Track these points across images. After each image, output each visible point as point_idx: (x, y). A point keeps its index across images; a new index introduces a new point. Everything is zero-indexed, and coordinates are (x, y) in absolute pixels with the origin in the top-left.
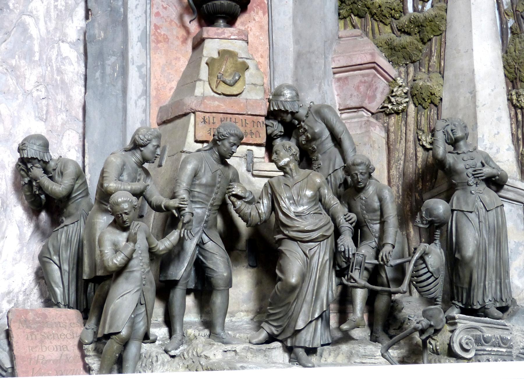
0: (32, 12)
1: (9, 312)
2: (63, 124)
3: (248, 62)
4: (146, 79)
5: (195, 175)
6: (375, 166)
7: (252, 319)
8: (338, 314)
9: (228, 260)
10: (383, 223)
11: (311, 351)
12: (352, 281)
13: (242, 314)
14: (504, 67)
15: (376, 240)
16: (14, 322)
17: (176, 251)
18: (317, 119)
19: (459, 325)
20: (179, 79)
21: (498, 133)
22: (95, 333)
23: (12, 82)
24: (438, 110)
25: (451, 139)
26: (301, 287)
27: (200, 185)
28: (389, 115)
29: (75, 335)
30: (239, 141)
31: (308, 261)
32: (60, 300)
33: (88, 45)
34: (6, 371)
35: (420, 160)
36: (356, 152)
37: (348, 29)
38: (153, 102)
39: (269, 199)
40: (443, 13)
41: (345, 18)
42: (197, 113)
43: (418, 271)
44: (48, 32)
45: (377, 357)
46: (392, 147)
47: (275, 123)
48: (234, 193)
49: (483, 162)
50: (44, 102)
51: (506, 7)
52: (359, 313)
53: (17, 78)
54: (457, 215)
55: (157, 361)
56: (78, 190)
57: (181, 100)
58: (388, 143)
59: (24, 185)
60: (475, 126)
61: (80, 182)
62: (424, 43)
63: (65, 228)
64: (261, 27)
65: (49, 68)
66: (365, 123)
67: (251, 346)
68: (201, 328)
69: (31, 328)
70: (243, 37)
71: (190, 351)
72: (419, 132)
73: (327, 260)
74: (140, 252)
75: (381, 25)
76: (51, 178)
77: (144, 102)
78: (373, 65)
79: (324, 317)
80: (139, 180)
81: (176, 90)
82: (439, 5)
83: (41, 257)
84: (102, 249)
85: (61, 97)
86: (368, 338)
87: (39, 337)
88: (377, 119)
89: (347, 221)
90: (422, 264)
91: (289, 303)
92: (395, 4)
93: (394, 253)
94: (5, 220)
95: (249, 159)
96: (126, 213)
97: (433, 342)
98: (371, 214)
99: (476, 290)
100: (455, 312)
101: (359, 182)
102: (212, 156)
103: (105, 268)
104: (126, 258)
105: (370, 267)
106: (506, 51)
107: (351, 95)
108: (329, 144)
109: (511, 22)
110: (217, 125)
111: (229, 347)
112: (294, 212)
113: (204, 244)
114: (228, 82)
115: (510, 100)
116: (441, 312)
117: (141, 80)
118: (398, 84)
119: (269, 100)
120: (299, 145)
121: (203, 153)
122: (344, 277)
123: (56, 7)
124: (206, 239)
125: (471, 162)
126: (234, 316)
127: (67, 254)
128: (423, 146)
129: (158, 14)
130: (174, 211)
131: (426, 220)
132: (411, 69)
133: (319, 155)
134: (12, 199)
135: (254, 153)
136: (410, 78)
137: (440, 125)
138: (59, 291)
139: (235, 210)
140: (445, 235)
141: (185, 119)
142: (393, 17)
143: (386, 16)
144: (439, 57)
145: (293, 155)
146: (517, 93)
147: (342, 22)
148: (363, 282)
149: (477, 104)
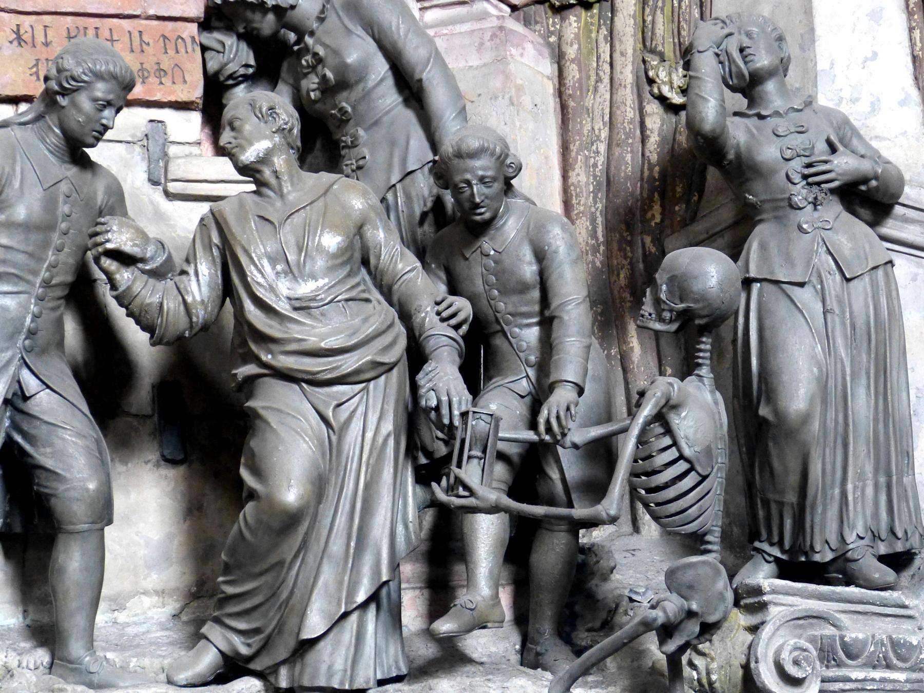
8: (426, 592)
9: (97, 442)
10: (547, 322)
12: (461, 491)
13: (147, 601)
15: (531, 373)
19: (773, 610)
25: (741, 75)
31: (334, 438)
35: (654, 139)
46: (572, 104)
47: (230, 41)
48: (109, 246)
49: (833, 138)
58: (560, 93)
72: (649, 57)
73: (388, 435)
86: (515, 658)
91: (281, 563)
97: (699, 662)
98: (515, 298)
100: (761, 575)
101: (478, 206)
102: (43, 140)
105: (513, 450)
110: (59, 46)
112: (289, 299)
113: (26, 398)
116: (718, 573)
120: (300, 104)
124: (31, 383)
125: (797, 141)
126: (121, 608)
131: (671, 311)
133: (361, 132)
139: (117, 298)
145: (280, 130)
148: (493, 495)
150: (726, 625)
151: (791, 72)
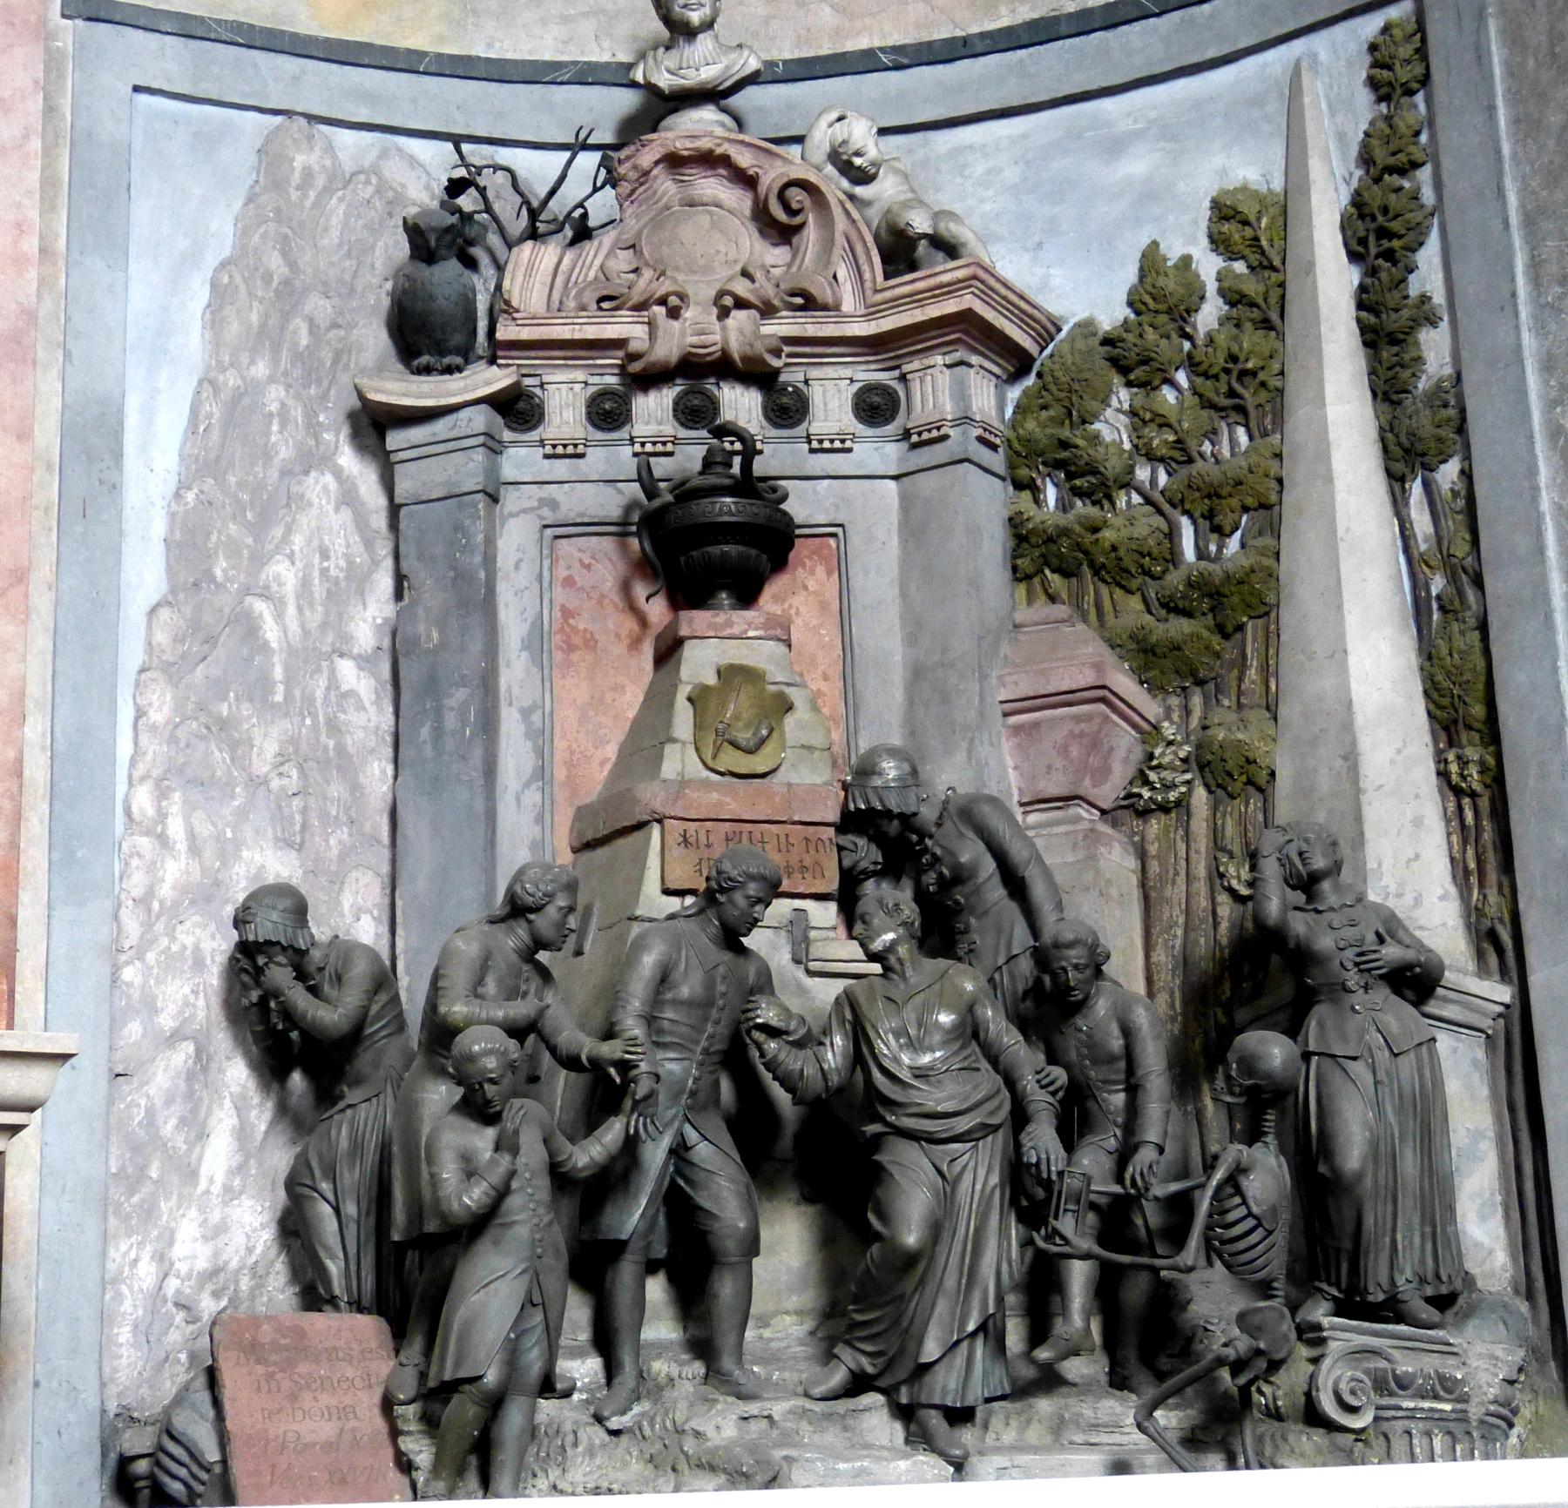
0: (267, 587)
1: (214, 1323)
2: (343, 855)
3: (792, 693)
4: (542, 739)
5: (664, 978)
6: (1110, 946)
7: (812, 1333)
8: (1027, 1320)
9: (747, 1186)
10: (1133, 1089)
11: (960, 1416)
12: (1058, 1241)
13: (788, 1319)
14: (1426, 693)
15: (1119, 1132)
16: (226, 1349)
17: (619, 1167)
18: (964, 830)
19: (1333, 1345)
20: (622, 737)
21: (1417, 857)
22: (423, 1376)
23: (220, 757)
24: (1265, 800)
25: (1299, 876)
26: (932, 1259)
27: (677, 1003)
28: (1144, 814)
29: (373, 1380)
30: (773, 890)
31: (948, 1189)
32: (337, 1291)
33: (401, 660)
34: (208, 1471)
35: (1224, 926)
36: (1062, 911)
37: (1037, 605)
38: (561, 795)
39: (846, 1034)
40: (1270, 562)
41: (1028, 578)
42: (668, 822)
43: (1227, 1211)
44: (306, 633)
45: (1126, 1430)
46: (1153, 894)
47: (862, 842)
48: (759, 1021)
49: (1381, 930)
50: (297, 803)
51: (1423, 547)
52: (1077, 1320)
53: (233, 746)
54: (1318, 1066)
55: (575, 1444)
56: (378, 1017)
57: (629, 790)
58: (1143, 884)
59: (247, 1009)
60: (1359, 840)
61: (383, 998)
62: (1226, 636)
63: (349, 1112)
64: (823, 607)
65: (308, 722)
66: (1085, 837)
67: (809, 1404)
68: (685, 1357)
69: (267, 1363)
70: (778, 632)
71: (658, 1419)
72: (1219, 855)
73: (994, 1188)
74: (527, 1175)
75: (1118, 593)
76: (314, 991)
77: (538, 797)
78: (1101, 693)
79: (991, 1331)
80: (525, 994)
81: (616, 765)
82: (1259, 542)
83: (292, 1184)
84: (435, 1169)
85: (337, 789)
86: (1104, 1379)
87: (286, 1385)
88: (1115, 824)
89: (1042, 1087)
90: (1232, 1196)
91: (901, 1297)
92: (1151, 542)
93: (1162, 1166)
94: (205, 1094)
95: (799, 932)
96: (492, 1081)
97: (1266, 1389)
98: (1104, 1068)
99: (1372, 1256)
100: (1321, 1311)
101: (1073, 989)
102: (704, 930)
103: (443, 1217)
104: (493, 1193)
105: (1103, 1200)
106: (1427, 654)
107: (1049, 767)
108: (996, 892)
109: (1438, 584)
110: (718, 850)
111: (753, 1408)
112: (911, 1068)
113: (688, 1149)
114: (743, 744)
115: (1443, 774)
116: (1282, 1316)
117: (529, 744)
118: (1163, 739)
119: (845, 787)
120: (921, 897)
121: (680, 924)
122: (1038, 1231)
123: (324, 572)
124: (692, 1135)
125: (1349, 933)
126: (767, 1325)
127: (353, 1177)
128: (1232, 892)
129: (569, 582)
130: (612, 1071)
131: (1240, 1085)
132: (1197, 700)
133: (973, 921)
134: (222, 1039)
135: (811, 917)
136: (1194, 722)
137: (1269, 842)
138: (334, 1268)
139: (764, 1064)
140: (1289, 1121)
141: (637, 836)
142: (1147, 573)
143: (1129, 572)
144: (1265, 669)
145: (904, 924)
146: (1459, 758)
147: (1021, 589)
148: (1086, 1244)
149: (1362, 785)
150: (1290, 1362)
151: (1344, 871)
